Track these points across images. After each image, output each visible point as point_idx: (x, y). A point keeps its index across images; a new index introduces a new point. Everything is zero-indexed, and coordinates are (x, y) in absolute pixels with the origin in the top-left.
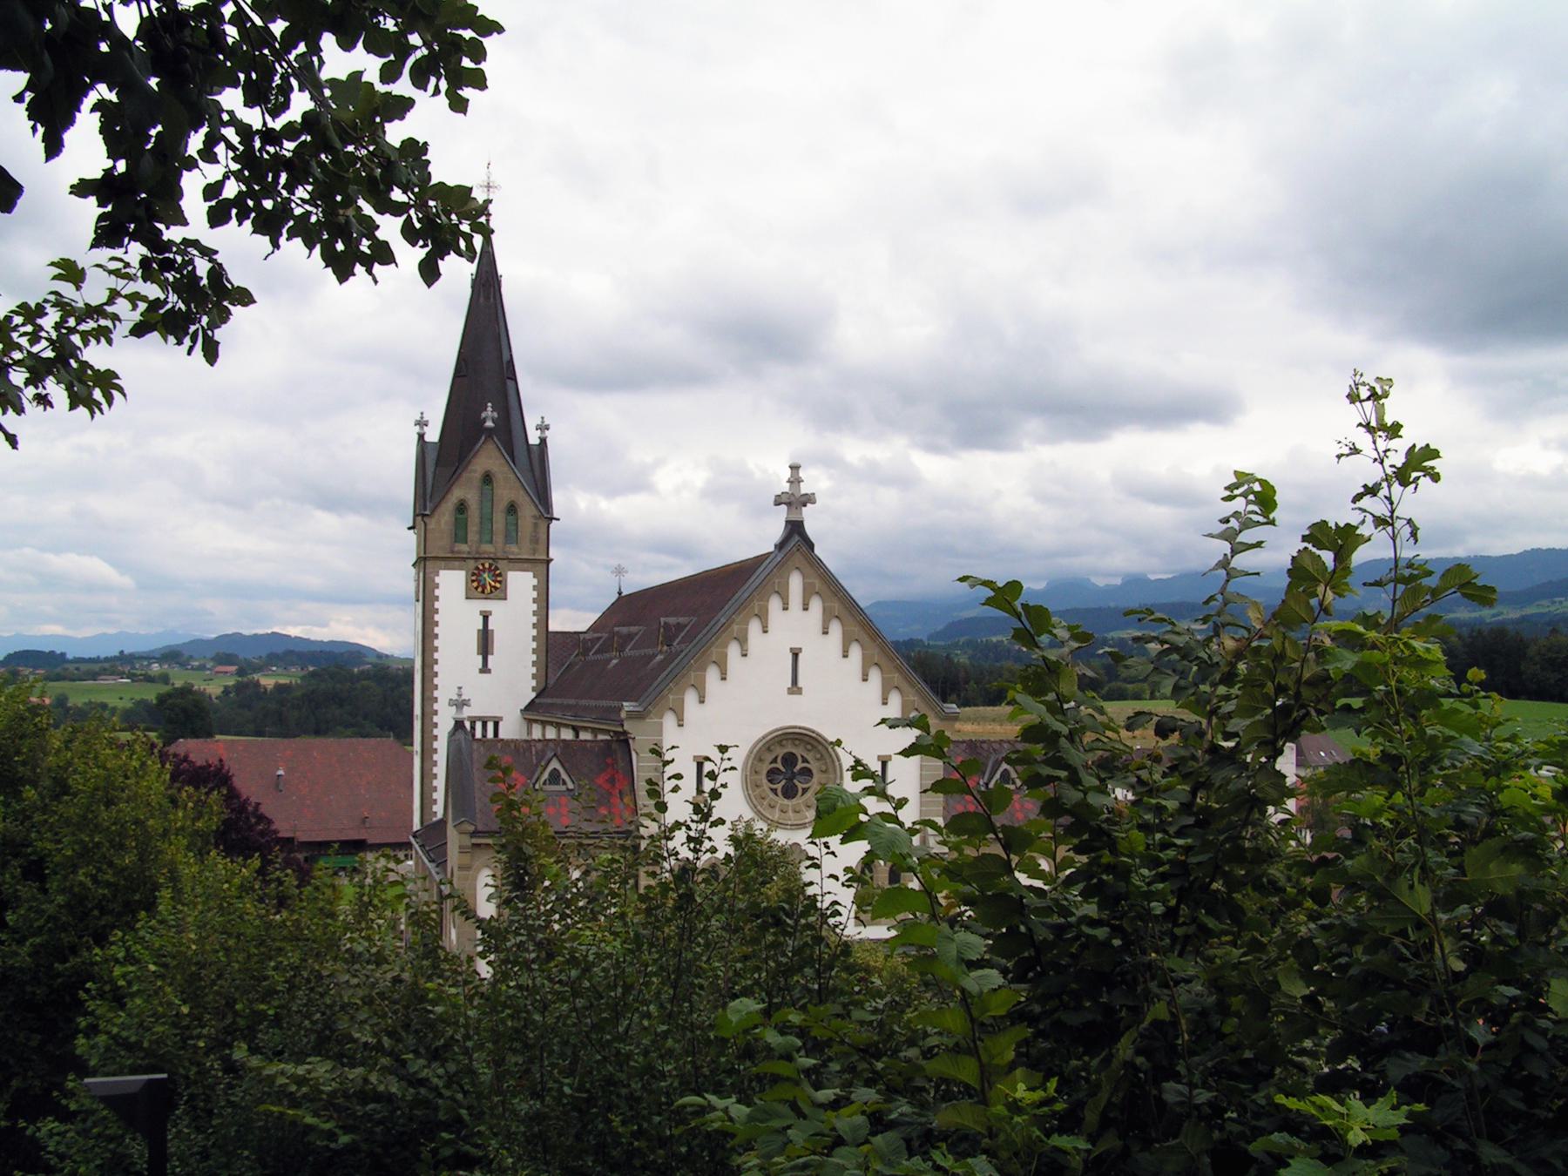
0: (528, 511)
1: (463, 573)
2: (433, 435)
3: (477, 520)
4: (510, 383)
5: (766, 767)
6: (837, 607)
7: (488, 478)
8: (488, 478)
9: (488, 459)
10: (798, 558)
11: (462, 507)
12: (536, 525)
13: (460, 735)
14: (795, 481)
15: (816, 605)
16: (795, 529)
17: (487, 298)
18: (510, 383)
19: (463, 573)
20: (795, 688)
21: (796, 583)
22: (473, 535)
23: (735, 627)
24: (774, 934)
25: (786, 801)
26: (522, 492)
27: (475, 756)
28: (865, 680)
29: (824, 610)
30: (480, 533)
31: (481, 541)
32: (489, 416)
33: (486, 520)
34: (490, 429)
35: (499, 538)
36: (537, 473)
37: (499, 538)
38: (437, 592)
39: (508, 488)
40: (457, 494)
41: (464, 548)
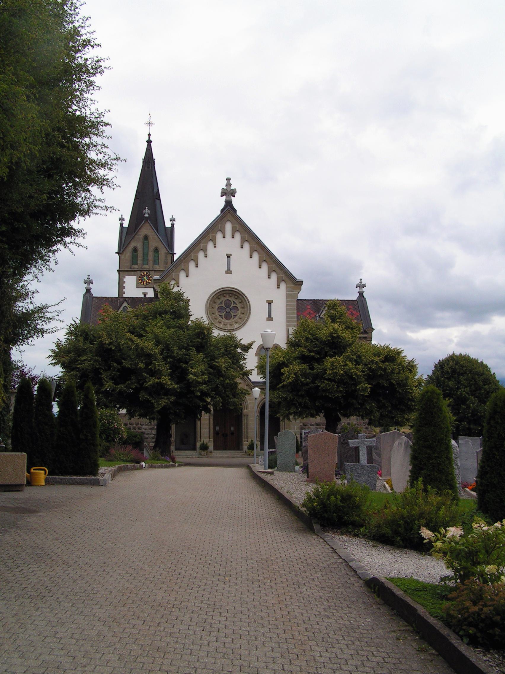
0: (163, 251)
1: (135, 277)
2: (126, 224)
3: (141, 255)
4: (157, 201)
5: (217, 306)
6: (247, 236)
7: (146, 238)
8: (146, 238)
9: (146, 230)
10: (229, 216)
11: (135, 250)
12: (166, 257)
13: (88, 295)
14: (229, 185)
15: (238, 236)
16: (229, 204)
17: (148, 167)
18: (157, 201)
19: (135, 277)
20: (229, 271)
21: (228, 227)
22: (140, 261)
23: (201, 245)
24: (451, 622)
25: (226, 321)
26: (160, 243)
27: (94, 303)
28: (278, 288)
29: (250, 247)
30: (143, 260)
31: (143, 264)
32: (147, 212)
33: (145, 255)
34: (146, 217)
35: (151, 262)
36: (169, 238)
37: (151, 262)
38: (124, 285)
39: (155, 242)
40: (133, 244)
41: (136, 267)
